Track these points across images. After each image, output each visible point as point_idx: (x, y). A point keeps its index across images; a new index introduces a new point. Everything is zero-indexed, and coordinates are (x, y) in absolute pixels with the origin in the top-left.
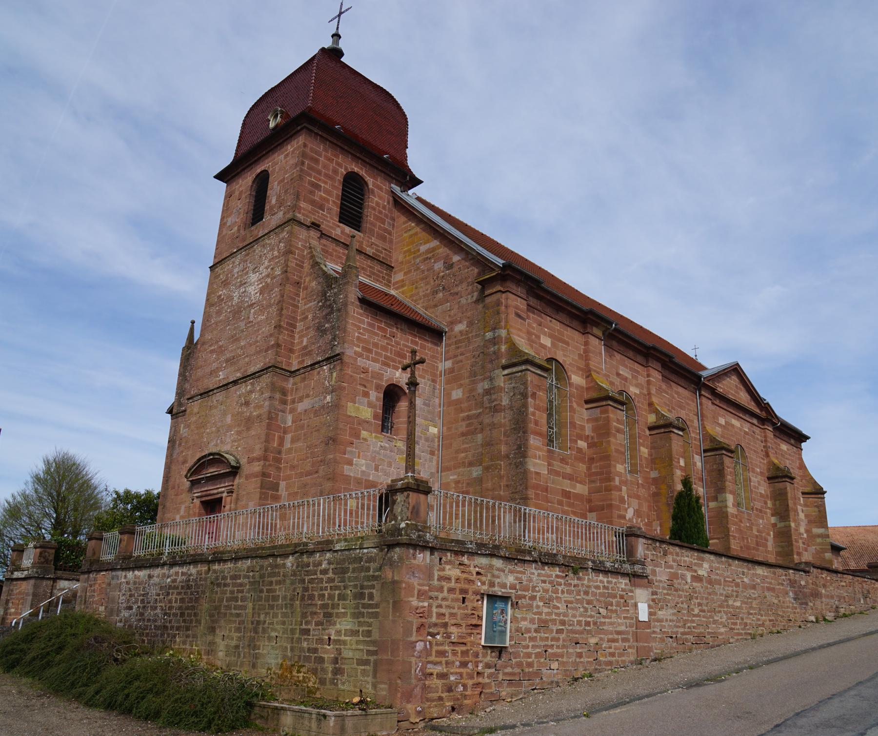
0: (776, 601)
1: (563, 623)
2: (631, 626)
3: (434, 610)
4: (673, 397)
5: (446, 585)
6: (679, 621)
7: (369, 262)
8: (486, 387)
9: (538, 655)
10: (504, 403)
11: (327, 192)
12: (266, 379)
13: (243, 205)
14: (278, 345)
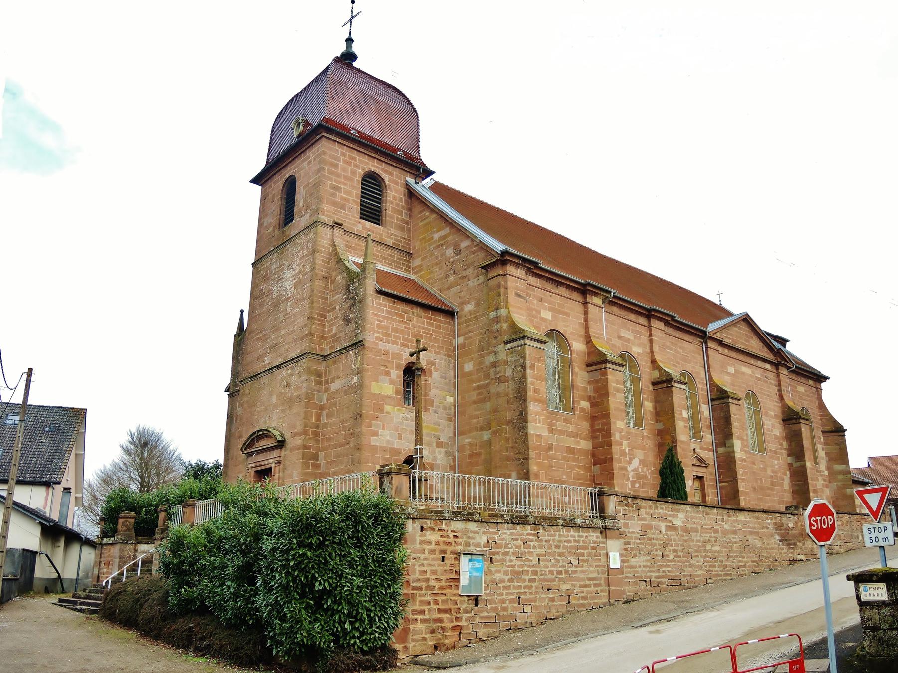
0: (758, 543)
1: (535, 573)
2: (603, 573)
3: (417, 568)
4: (679, 353)
5: (427, 548)
6: (653, 567)
7: (389, 251)
8: (492, 361)
9: (512, 601)
10: (507, 375)
11: (346, 192)
12: (303, 364)
13: (276, 207)
14: (311, 334)
